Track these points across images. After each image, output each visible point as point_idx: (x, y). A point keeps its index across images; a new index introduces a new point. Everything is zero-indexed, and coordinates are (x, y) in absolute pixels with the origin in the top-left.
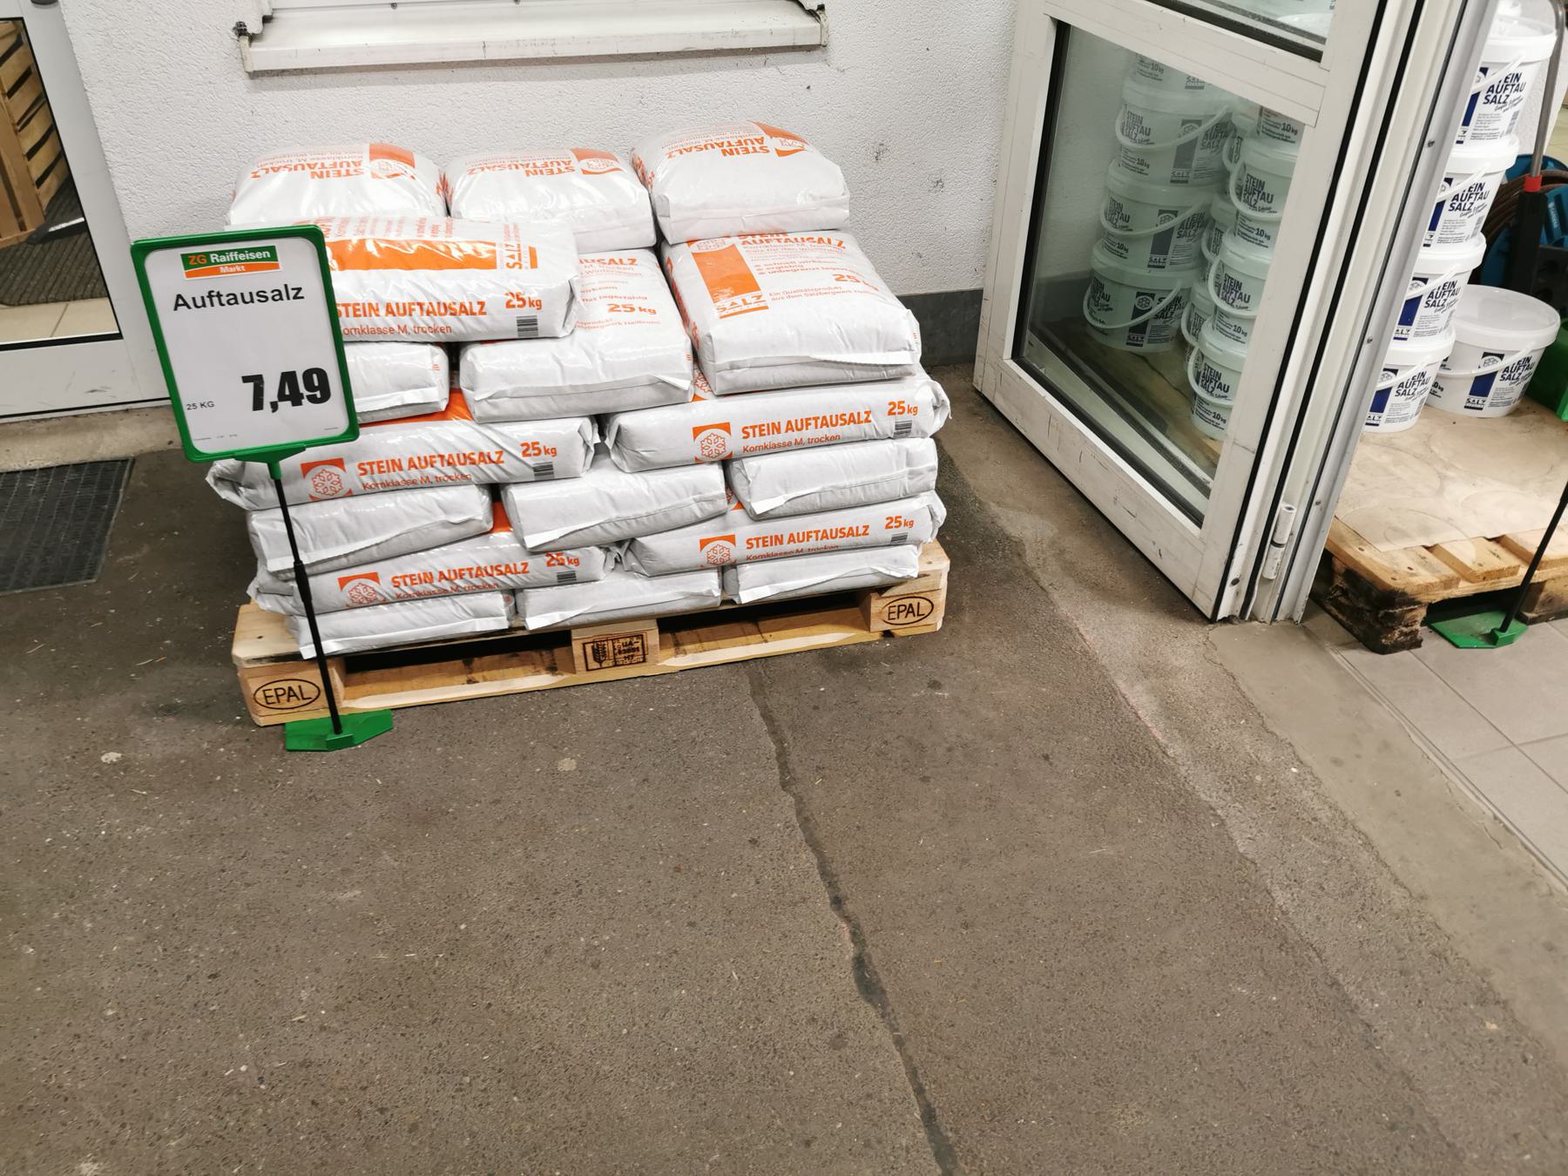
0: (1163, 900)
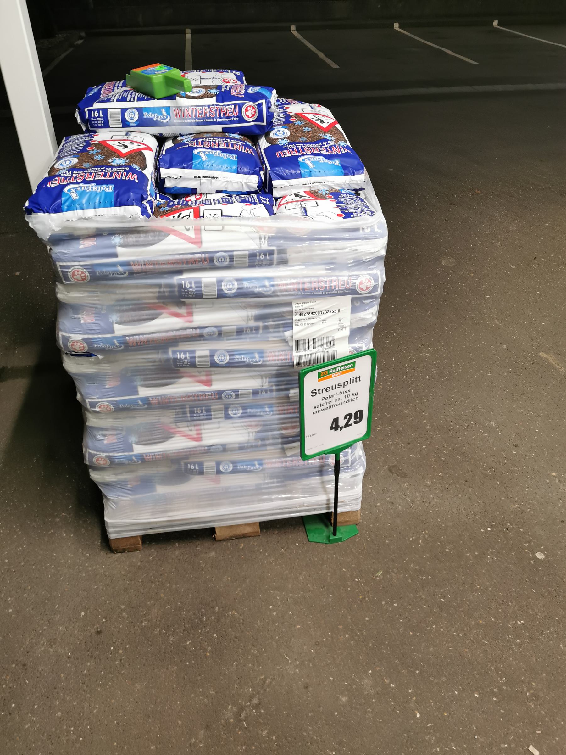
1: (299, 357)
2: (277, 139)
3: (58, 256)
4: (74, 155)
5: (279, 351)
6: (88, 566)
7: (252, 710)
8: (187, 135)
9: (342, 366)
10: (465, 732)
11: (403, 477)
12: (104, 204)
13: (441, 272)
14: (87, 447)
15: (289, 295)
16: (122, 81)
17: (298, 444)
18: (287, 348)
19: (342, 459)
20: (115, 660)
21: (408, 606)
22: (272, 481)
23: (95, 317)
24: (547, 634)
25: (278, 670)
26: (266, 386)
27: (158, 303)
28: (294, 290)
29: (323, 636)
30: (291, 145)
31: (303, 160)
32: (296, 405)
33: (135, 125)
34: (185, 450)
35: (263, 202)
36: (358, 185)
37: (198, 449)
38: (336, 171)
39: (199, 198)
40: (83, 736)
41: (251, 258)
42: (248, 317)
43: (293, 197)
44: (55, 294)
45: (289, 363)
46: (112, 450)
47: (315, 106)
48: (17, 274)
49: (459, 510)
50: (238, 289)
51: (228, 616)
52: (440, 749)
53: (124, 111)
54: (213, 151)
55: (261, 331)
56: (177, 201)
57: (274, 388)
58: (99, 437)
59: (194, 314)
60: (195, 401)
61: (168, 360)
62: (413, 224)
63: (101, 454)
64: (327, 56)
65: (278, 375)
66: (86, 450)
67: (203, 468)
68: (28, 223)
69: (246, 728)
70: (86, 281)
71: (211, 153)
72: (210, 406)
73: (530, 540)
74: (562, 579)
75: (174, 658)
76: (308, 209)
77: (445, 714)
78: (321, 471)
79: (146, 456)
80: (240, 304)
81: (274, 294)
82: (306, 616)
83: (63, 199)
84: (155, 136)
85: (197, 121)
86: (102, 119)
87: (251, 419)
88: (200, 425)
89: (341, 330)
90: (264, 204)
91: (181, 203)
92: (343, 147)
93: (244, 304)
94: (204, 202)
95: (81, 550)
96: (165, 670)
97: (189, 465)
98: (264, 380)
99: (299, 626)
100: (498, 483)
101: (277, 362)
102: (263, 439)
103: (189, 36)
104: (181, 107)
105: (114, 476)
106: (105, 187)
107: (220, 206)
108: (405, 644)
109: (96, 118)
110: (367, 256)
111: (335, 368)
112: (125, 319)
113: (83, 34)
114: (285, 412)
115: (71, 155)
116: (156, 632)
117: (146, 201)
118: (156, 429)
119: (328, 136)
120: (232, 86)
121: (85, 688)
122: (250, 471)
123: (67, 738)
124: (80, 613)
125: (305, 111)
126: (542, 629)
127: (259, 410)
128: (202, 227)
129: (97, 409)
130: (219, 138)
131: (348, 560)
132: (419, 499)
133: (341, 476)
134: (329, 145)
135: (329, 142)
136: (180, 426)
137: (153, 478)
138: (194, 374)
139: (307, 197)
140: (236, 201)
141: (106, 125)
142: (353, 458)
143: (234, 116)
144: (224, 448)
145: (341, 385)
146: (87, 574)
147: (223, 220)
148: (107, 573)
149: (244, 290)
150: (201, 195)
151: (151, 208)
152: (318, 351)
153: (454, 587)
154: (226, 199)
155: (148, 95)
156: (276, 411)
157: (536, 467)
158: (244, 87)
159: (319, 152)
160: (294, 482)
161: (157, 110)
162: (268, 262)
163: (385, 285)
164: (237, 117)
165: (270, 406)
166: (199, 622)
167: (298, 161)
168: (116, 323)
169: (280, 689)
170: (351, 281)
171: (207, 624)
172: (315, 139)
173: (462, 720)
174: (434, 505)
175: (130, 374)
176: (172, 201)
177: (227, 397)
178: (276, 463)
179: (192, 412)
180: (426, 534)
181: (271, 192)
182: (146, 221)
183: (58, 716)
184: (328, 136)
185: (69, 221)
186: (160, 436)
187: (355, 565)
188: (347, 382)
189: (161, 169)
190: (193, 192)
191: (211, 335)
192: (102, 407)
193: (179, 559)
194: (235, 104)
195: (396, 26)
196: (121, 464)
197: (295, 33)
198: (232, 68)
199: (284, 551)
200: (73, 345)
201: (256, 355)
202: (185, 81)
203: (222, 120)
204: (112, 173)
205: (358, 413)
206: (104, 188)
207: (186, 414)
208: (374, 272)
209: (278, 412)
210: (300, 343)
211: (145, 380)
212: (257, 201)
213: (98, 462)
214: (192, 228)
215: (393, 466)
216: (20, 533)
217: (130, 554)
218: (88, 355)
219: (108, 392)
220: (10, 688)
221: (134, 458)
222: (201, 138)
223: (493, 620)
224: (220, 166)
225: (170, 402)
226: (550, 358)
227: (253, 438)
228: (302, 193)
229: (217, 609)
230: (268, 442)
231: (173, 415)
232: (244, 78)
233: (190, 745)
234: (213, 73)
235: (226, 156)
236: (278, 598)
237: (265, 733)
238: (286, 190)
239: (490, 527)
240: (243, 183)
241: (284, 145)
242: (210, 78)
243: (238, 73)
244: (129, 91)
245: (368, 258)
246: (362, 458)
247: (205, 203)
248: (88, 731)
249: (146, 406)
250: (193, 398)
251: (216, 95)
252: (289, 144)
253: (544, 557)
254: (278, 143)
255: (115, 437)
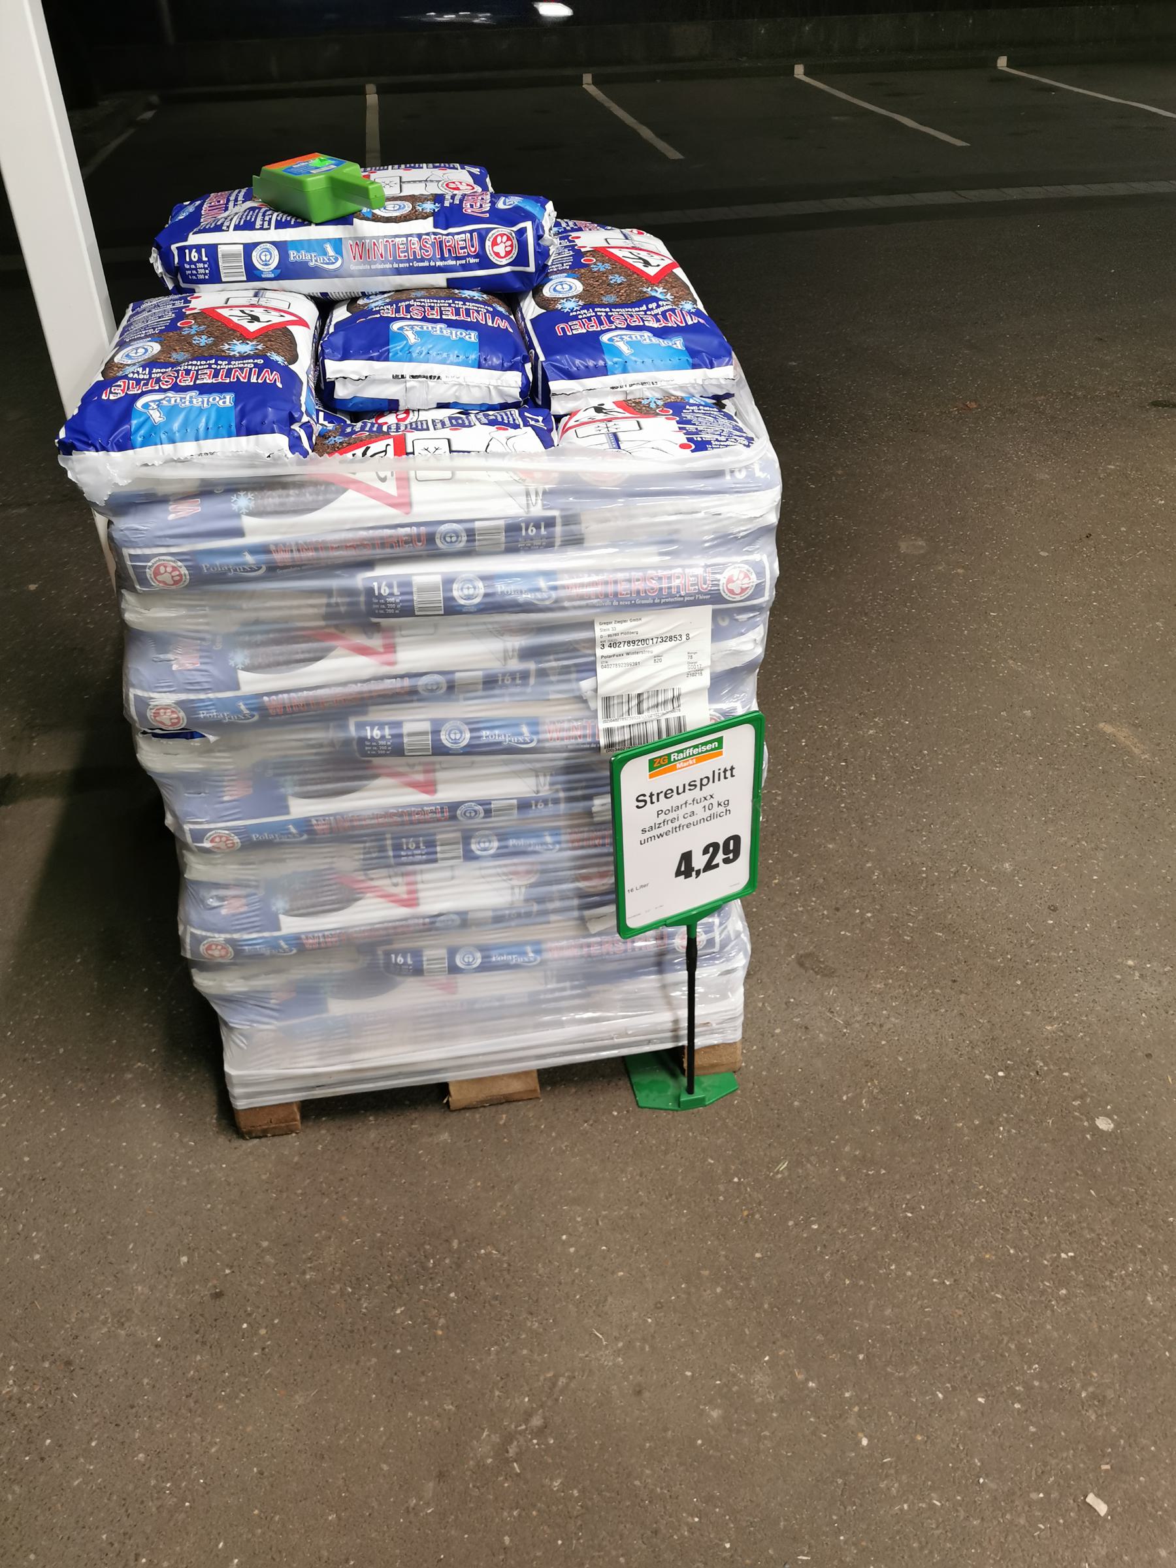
0: (445, 1544)
1: (609, 732)
2: (556, 300)
3: (126, 536)
4: (153, 338)
5: (569, 721)
6: (192, 1166)
7: (531, 1440)
8: (376, 295)
9: (696, 746)
10: (959, 1472)
11: (826, 975)
12: (216, 431)
13: (898, 567)
14: (188, 923)
15: (588, 606)
16: (244, 191)
17: (612, 909)
18: (587, 713)
19: (701, 939)
20: (252, 1349)
21: (839, 1227)
22: (562, 985)
23: (201, 657)
24: (1121, 1276)
25: (581, 1359)
26: (545, 791)
27: (327, 626)
28: (597, 597)
29: (671, 1290)
30: (586, 311)
31: (611, 339)
32: (605, 830)
33: (273, 276)
34: (386, 925)
35: (532, 423)
36: (719, 386)
37: (411, 922)
38: (675, 360)
39: (404, 420)
40: (190, 1498)
41: (509, 534)
42: (505, 651)
43: (592, 412)
44: (119, 613)
45: (590, 743)
46: (238, 927)
47: (633, 233)
48: (32, 587)
49: (940, 1040)
50: (486, 595)
51: (479, 1257)
52: (909, 1506)
53: (249, 248)
54: (430, 325)
55: (532, 681)
56: (359, 424)
57: (562, 795)
58: (212, 902)
59: (398, 648)
60: (403, 824)
61: (347, 742)
62: (840, 472)
63: (216, 935)
64: (661, 135)
65: (568, 770)
66: (185, 929)
67: (422, 961)
68: (64, 472)
69: (518, 1475)
70: (181, 585)
71: (425, 328)
72: (435, 834)
73: (1085, 1093)
74: (1150, 1169)
75: (371, 1342)
76: (621, 436)
77: (919, 1438)
78: (660, 962)
79: (307, 938)
80: (490, 626)
81: (557, 606)
82: (636, 1253)
83: (134, 422)
84: (313, 298)
85: (396, 265)
86: (206, 266)
87: (516, 860)
88: (414, 873)
89: (693, 675)
90: (533, 427)
91: (367, 429)
92: (690, 313)
93: (496, 626)
94: (414, 426)
95: (177, 1135)
96: (353, 1366)
97: (393, 956)
98: (542, 779)
99: (621, 1274)
100: (1019, 982)
101: (566, 742)
102: (540, 900)
103: (372, 99)
104: (364, 238)
105: (242, 980)
106: (218, 399)
107: (447, 433)
108: (837, 1302)
109: (195, 263)
110: (742, 525)
111: (681, 751)
112: (260, 660)
113: (154, 99)
114: (585, 843)
115: (146, 336)
116: (333, 1292)
117: (299, 424)
118: (325, 883)
119: (659, 292)
120: (464, 196)
121: (193, 1404)
122: (516, 967)
123: (159, 1503)
124: (179, 1257)
125: (613, 243)
126: (1111, 1267)
127: (532, 841)
128: (412, 474)
129: (207, 844)
130: (440, 298)
131: (719, 1142)
132: (859, 1018)
133: (698, 973)
134: (662, 309)
135: (660, 303)
136: (373, 876)
137: (322, 984)
138: (401, 769)
139: (619, 412)
140: (477, 423)
141: (214, 277)
142: (723, 936)
143: (469, 256)
144: (465, 921)
145: (695, 786)
146: (191, 1181)
147: (451, 458)
148: (232, 1179)
149: (497, 599)
150: (407, 412)
151: (310, 438)
152: (647, 719)
153: (933, 1188)
154: (457, 419)
155: (298, 217)
156: (568, 842)
157: (1095, 950)
158: (488, 197)
159: (642, 324)
160: (606, 987)
161: (316, 246)
162: (545, 541)
163: (780, 584)
164: (475, 257)
165: (555, 831)
166: (420, 1270)
167: (599, 342)
168: (243, 669)
169: (586, 1396)
170: (709, 577)
171: (437, 1273)
172: (634, 297)
173: (953, 1449)
174: (889, 1029)
175: (270, 772)
176: (349, 425)
177: (468, 815)
178: (568, 947)
179: (397, 847)
180: (875, 1086)
181: (547, 404)
182: (299, 463)
183: (138, 1461)
184: (659, 292)
185: (146, 465)
186: (333, 897)
187: (733, 1150)
188: (708, 778)
189: (326, 361)
190: (392, 406)
191: (432, 690)
192: (217, 840)
193: (377, 1149)
194: (471, 232)
195: (799, 71)
196: (256, 957)
197: (592, 90)
198: (463, 159)
199: (588, 1127)
200: (157, 714)
201: (525, 729)
202: (370, 187)
203: (446, 263)
204: (229, 371)
205: (732, 842)
206: (214, 399)
207: (386, 851)
208: (756, 557)
209: (570, 845)
210: (611, 703)
211: (303, 783)
212: (519, 421)
213: (210, 952)
214: (392, 475)
215: (809, 955)
216: (52, 1103)
217: (276, 1139)
218: (187, 734)
219: (227, 809)
220: (41, 1408)
221: (282, 943)
222: (405, 301)
223: (1012, 1251)
224: (445, 355)
225: (353, 828)
226: (1123, 734)
227: (522, 898)
228: (609, 405)
229: (455, 1244)
230: (551, 906)
231: (360, 854)
232: (488, 180)
233: (408, 1511)
234: (425, 171)
235: (455, 334)
236: (579, 1219)
237: (556, 1484)
238: (576, 399)
239: (1002, 1071)
240: (491, 388)
241: (572, 311)
242: (420, 181)
243: (476, 171)
244: (260, 208)
245: (742, 529)
246: (742, 936)
247: (415, 427)
248: (200, 1489)
249: (305, 837)
250: (399, 819)
251: (434, 214)
252: (581, 309)
253: (1112, 1126)
254: (559, 307)
255: (244, 901)
